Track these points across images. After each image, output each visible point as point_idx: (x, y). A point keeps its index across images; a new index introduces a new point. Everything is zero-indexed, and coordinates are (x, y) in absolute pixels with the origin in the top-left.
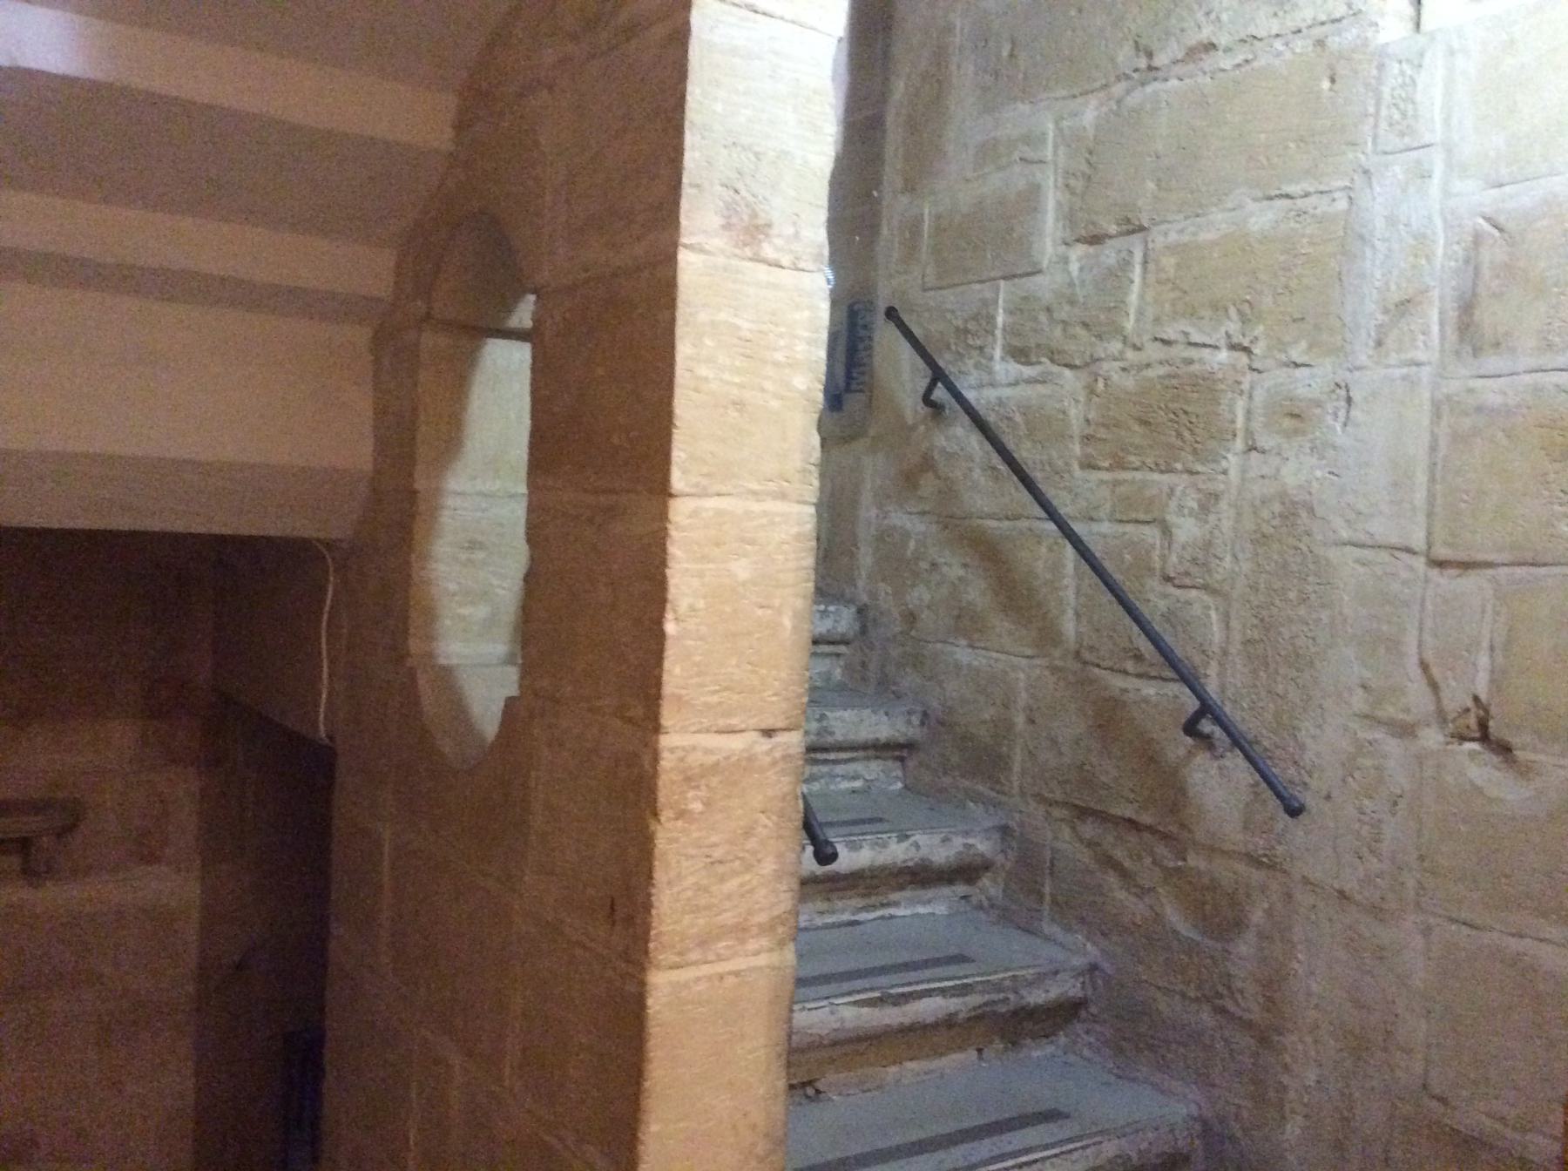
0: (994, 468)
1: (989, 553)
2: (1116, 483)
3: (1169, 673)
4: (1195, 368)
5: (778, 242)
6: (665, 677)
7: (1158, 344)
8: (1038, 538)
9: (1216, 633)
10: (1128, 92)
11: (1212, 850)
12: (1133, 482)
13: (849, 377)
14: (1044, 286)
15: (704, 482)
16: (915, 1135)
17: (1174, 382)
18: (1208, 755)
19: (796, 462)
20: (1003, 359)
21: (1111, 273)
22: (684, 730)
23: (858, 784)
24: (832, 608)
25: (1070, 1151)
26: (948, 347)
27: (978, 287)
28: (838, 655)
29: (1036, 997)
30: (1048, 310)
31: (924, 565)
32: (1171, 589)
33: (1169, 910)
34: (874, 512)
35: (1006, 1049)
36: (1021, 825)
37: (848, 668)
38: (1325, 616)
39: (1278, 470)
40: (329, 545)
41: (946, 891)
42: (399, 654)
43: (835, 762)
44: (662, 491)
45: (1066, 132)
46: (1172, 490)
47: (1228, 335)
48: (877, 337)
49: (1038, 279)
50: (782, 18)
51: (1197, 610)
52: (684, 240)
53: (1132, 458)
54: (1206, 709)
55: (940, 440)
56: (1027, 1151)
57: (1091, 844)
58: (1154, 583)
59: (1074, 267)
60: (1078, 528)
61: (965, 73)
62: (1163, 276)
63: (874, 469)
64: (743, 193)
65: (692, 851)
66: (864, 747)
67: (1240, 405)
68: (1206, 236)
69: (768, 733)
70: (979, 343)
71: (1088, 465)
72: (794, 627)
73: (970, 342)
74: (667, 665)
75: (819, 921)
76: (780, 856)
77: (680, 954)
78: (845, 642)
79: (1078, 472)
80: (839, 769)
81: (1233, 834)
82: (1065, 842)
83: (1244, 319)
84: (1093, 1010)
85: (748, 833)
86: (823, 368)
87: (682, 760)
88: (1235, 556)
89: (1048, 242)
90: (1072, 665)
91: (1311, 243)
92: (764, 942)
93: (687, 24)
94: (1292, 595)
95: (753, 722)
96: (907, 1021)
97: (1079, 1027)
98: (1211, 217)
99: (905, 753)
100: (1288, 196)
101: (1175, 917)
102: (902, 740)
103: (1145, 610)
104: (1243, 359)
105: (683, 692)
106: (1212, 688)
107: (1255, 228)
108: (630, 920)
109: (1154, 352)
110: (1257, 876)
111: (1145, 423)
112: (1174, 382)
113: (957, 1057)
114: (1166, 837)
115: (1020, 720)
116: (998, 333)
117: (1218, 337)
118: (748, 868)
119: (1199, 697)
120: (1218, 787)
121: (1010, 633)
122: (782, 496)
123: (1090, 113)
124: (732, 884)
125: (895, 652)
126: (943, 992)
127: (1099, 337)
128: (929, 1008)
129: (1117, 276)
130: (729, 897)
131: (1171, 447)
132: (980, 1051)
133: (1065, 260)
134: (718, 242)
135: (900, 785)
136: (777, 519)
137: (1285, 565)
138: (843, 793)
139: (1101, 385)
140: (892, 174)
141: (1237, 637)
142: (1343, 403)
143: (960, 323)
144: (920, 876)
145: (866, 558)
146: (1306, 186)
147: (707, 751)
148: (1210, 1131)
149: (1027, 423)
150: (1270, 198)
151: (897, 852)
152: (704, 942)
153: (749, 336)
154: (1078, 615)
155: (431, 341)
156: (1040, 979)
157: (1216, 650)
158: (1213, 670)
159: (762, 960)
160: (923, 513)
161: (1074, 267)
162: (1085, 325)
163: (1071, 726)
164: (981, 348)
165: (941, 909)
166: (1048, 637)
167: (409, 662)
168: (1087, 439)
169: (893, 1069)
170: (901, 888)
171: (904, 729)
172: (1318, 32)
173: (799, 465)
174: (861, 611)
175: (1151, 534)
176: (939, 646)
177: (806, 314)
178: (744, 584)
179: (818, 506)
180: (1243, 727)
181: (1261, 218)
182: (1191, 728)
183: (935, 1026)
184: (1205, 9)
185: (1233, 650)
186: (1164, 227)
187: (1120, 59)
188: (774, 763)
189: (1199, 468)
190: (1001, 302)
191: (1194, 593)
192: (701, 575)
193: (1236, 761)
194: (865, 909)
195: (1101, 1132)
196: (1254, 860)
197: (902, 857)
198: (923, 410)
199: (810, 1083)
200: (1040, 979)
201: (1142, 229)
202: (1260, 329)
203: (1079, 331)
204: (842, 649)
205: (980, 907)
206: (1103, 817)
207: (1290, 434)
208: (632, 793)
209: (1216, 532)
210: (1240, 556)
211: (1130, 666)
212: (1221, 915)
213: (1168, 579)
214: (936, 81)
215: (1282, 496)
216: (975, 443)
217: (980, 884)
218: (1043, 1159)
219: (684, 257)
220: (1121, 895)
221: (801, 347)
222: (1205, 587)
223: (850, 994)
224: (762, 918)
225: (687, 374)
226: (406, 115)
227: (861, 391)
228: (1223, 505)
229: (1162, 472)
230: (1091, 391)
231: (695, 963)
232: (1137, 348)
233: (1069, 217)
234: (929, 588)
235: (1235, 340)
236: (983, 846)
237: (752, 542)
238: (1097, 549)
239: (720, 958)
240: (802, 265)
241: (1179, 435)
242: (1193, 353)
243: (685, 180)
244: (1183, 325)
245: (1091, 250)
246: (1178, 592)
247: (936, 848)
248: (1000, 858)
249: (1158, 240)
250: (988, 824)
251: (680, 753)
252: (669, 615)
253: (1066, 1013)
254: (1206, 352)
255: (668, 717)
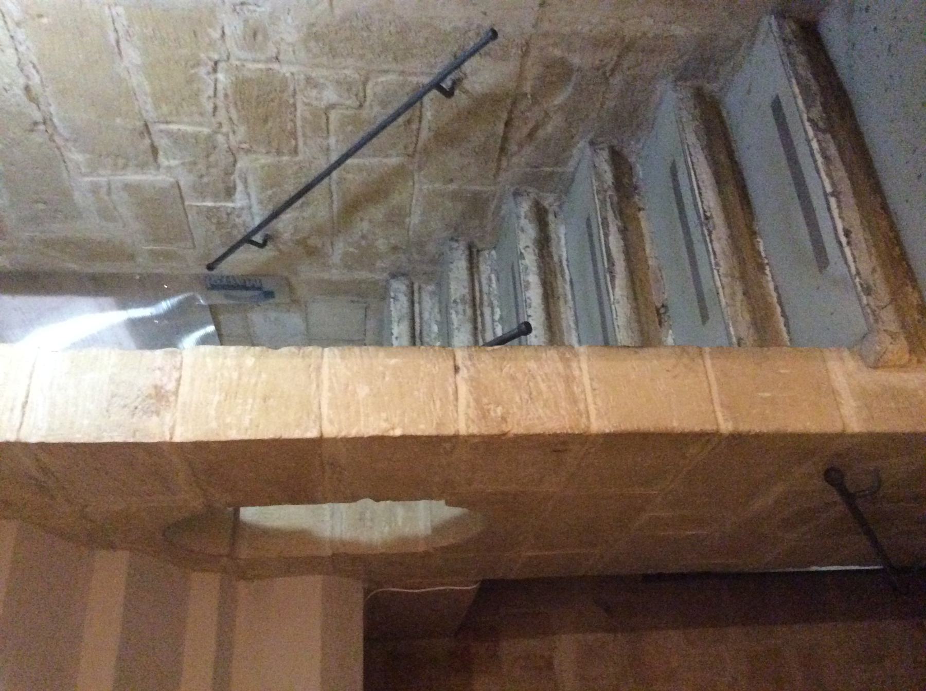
0: (302, 206)
1: (353, 207)
2: (304, 135)
3: (418, 104)
4: (229, 92)
5: (165, 380)
6: (427, 434)
7: (217, 113)
8: (341, 181)
9: (392, 77)
10: (60, 135)
11: (521, 76)
12: (303, 127)
13: (253, 288)
14: (186, 180)
15: (313, 417)
16: (685, 255)
17: (239, 103)
18: (465, 81)
19: (298, 362)
20: (233, 202)
21: (175, 142)
22: (456, 421)
23: (493, 277)
24: (392, 294)
25: (692, 163)
26: (229, 233)
27: (190, 217)
28: (420, 288)
29: (609, 177)
30: (201, 176)
31: (363, 243)
32: (367, 103)
33: (556, 103)
34: (334, 271)
35: (639, 194)
36: (512, 184)
37: (427, 284)
38: (377, 16)
39: (288, 44)
40: (367, 592)
41: (552, 226)
42: (426, 555)
43: (481, 291)
44: (319, 442)
45: (88, 170)
46: (306, 104)
47: (209, 73)
48: (226, 273)
49: (182, 183)
50: (29, 386)
51: (379, 89)
52: (167, 439)
53: (289, 127)
54: (436, 85)
55: (286, 236)
56: (692, 190)
57: (521, 146)
58: (365, 113)
59: (173, 163)
60: (334, 158)
61: (58, 229)
62: (174, 112)
63: (308, 272)
64: (136, 404)
65: (524, 412)
66: (472, 275)
67: (250, 65)
68: (148, 89)
69: (456, 369)
70: (225, 216)
71: (295, 151)
72: (396, 357)
73: (225, 220)
74: (419, 433)
75: (571, 303)
76: (526, 359)
77: (581, 415)
78: (411, 286)
79: (300, 157)
80: (485, 289)
81: (510, 67)
82: (520, 160)
83: (198, 64)
84: (615, 142)
85: (513, 378)
86: (241, 348)
87: (473, 421)
88: (344, 68)
89: (160, 178)
90: (416, 160)
91: (146, 27)
92: (574, 365)
93: (37, 444)
94: (365, 34)
95: (451, 380)
96: (622, 257)
97: (625, 151)
98: (135, 85)
99: (475, 250)
100: (118, 42)
101: (560, 99)
102: (467, 252)
103: (379, 121)
104: (222, 65)
105: (435, 422)
106: (426, 80)
107: (139, 59)
108: (564, 443)
109: (222, 115)
110: (534, 53)
111: (266, 121)
112: (239, 103)
113: (643, 224)
114: (514, 103)
115: (452, 187)
116: (218, 204)
117: (210, 80)
118: (534, 377)
119: (429, 90)
120: (483, 76)
121: (400, 193)
122: (319, 369)
123: (76, 157)
124: (543, 386)
125: (416, 256)
126: (606, 235)
127: (215, 148)
128: (615, 243)
129: (178, 139)
130: (549, 387)
131: (280, 105)
132: (640, 209)
133: (169, 168)
134: (168, 417)
135: (493, 252)
136: (333, 371)
137: (347, 39)
138: (499, 287)
139: (244, 146)
140: (126, 268)
141: (394, 66)
142: (245, 8)
143: (213, 228)
144: (544, 243)
145: (363, 275)
146: (110, 28)
147: (468, 406)
148: (681, 77)
149: (272, 187)
150: (120, 53)
151: (530, 260)
152: (574, 401)
153: (223, 394)
154: (387, 156)
155: (244, 552)
156: (599, 176)
157: (401, 78)
158: (415, 79)
159: (584, 366)
160: (332, 244)
161: (173, 163)
162: (208, 156)
163: (453, 159)
164: (228, 214)
165: (562, 230)
166: (401, 172)
167: (431, 551)
168: (279, 153)
169: (650, 263)
170: (551, 257)
171: (461, 252)
172: (11, 25)
173: (300, 360)
174: (394, 276)
175: (334, 115)
176: (411, 233)
177: (208, 360)
178: (371, 389)
179: (324, 347)
180: (446, 62)
181: (132, 55)
182: (449, 94)
183: (625, 239)
184: (4, 93)
185: (401, 68)
186: (143, 112)
187: (40, 140)
188: (474, 365)
189: (292, 88)
190: (199, 204)
191: (369, 91)
192: (367, 415)
193: (467, 67)
194: (563, 276)
195: (682, 143)
196: (525, 54)
197: (534, 258)
198: (270, 246)
199: (658, 310)
200: (599, 176)
201: (146, 126)
202: (202, 56)
203: (212, 159)
204: (416, 287)
205: (560, 207)
206: (505, 139)
207: (266, 37)
208: (493, 446)
209: (331, 78)
210: (343, 65)
211: (414, 126)
212: (557, 73)
213: (361, 106)
214: (66, 245)
215: (305, 41)
216: (286, 216)
217: (547, 207)
218: (697, 180)
219: (177, 439)
220: (549, 129)
221: (229, 362)
222: (365, 84)
223: (608, 293)
224: (560, 366)
225: (249, 432)
226: (109, 578)
227: (260, 281)
228: (314, 75)
229: (296, 110)
230: (248, 151)
231: (587, 407)
232: (220, 124)
233: (142, 166)
234: (377, 240)
235: (211, 70)
236: (525, 207)
237: (347, 385)
238: (344, 149)
239: (583, 391)
240: (178, 364)
241: (272, 100)
242: (221, 94)
243: (131, 440)
244: (204, 100)
245: (161, 153)
246: (368, 100)
247: (527, 237)
248: (532, 196)
249: (150, 114)
250: (512, 204)
251: (470, 422)
252: (391, 433)
253: (618, 159)
254: (220, 87)
255: (449, 431)
